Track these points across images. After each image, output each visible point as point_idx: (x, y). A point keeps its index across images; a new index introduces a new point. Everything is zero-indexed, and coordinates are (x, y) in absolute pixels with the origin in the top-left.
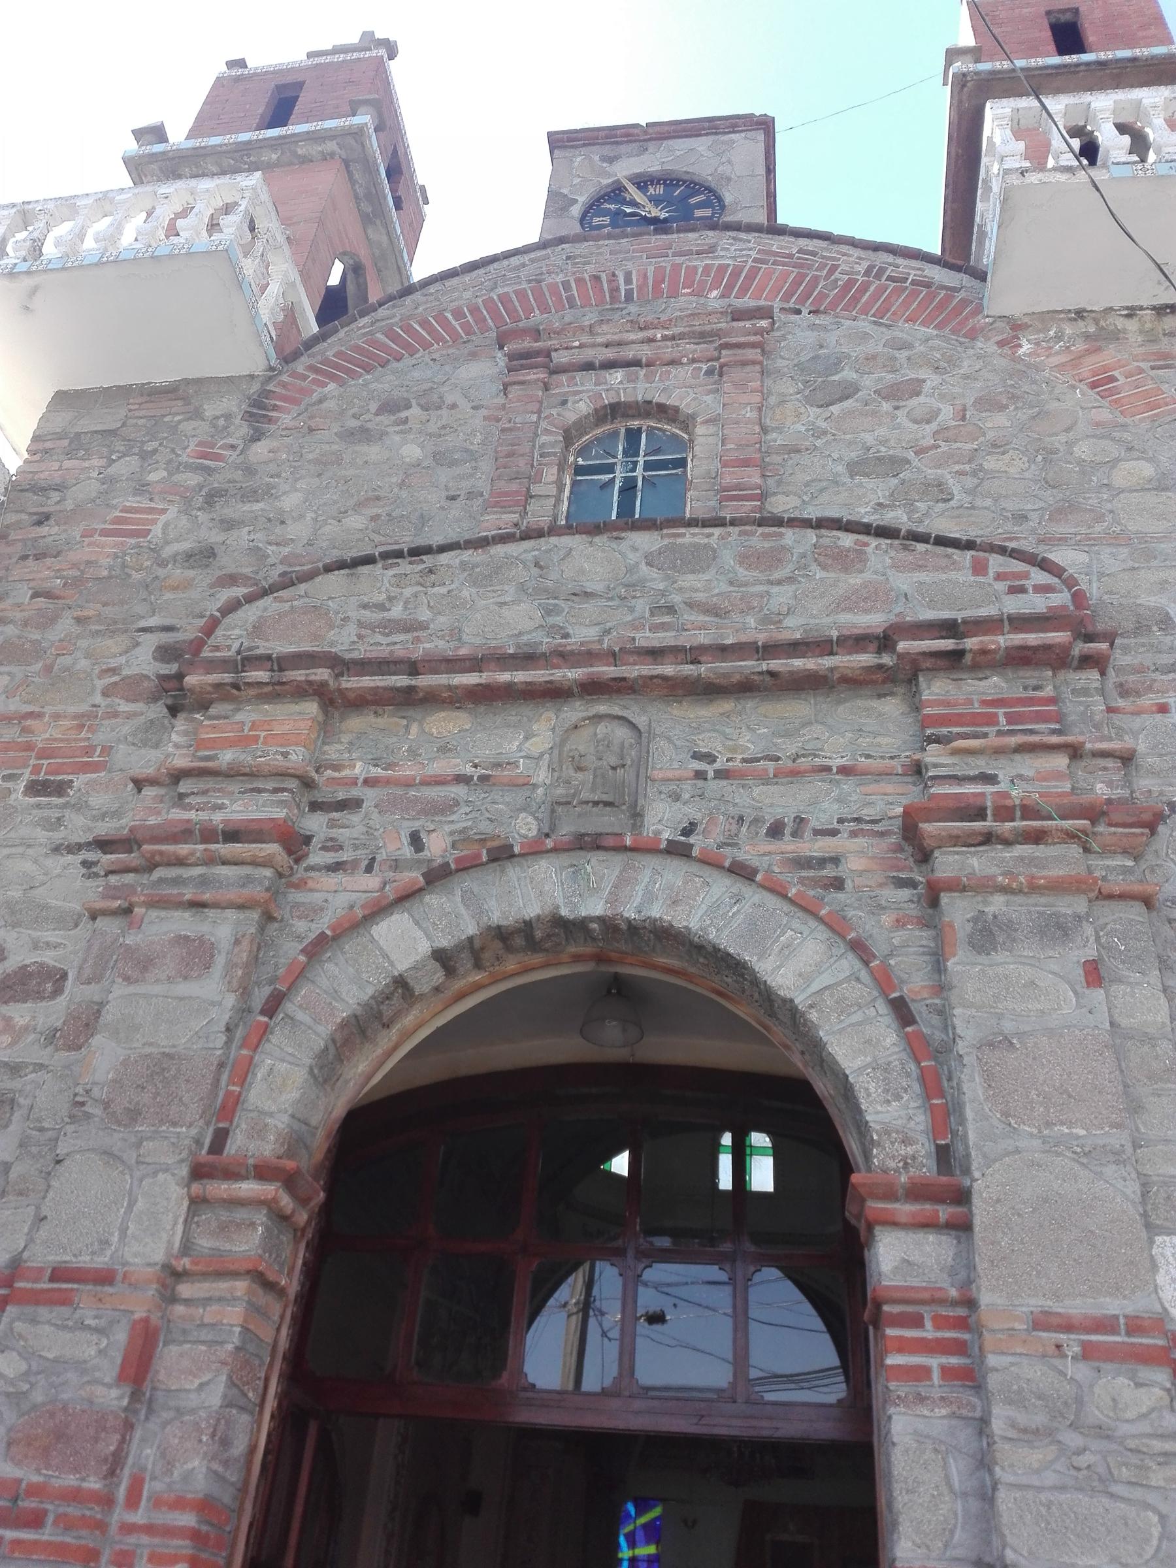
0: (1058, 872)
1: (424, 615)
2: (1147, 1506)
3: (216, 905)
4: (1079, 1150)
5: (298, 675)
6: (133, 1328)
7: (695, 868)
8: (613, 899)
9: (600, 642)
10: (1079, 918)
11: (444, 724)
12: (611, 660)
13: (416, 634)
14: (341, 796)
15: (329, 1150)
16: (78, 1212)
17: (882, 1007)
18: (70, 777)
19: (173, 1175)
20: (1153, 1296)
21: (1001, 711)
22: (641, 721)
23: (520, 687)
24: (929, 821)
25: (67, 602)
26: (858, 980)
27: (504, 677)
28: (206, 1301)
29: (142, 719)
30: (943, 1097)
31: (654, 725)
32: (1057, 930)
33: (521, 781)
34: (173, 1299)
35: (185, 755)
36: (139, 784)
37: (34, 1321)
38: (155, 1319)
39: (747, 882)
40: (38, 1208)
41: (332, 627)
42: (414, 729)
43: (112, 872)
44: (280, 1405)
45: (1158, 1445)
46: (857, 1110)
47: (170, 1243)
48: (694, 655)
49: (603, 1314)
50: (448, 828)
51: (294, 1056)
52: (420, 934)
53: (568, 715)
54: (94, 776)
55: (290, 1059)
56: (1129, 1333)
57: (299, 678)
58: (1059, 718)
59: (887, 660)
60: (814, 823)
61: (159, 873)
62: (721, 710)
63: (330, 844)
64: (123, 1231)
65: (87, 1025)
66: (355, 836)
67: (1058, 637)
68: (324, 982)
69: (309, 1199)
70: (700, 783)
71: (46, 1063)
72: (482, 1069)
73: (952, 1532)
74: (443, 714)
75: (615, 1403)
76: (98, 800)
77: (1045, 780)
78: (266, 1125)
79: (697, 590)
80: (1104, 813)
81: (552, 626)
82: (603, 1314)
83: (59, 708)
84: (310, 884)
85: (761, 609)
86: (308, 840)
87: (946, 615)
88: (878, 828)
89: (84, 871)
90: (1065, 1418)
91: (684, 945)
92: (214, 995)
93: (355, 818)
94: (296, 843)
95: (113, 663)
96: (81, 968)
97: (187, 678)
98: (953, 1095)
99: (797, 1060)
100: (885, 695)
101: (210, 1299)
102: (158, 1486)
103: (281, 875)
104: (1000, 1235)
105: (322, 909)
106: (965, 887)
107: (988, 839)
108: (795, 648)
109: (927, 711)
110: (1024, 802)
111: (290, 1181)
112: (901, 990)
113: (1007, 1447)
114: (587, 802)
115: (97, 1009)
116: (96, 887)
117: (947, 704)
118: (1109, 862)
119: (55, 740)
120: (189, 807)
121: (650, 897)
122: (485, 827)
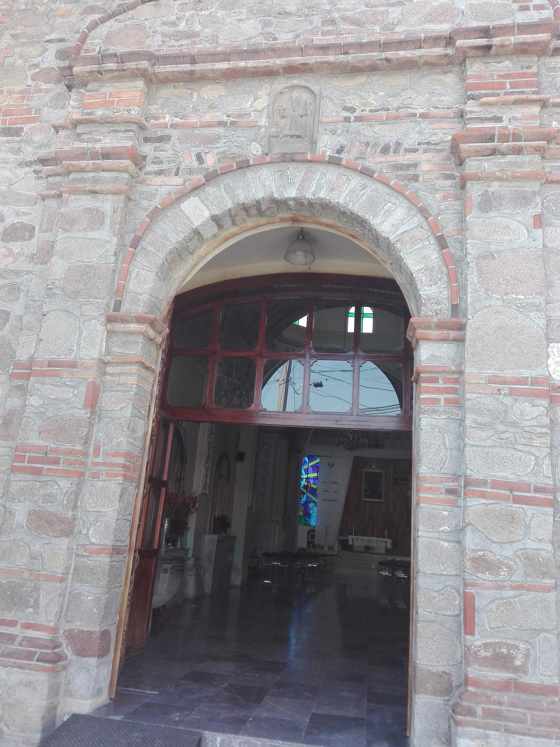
0: (527, 169)
1: (198, 28)
2: (530, 453)
3: (102, 193)
4: (519, 305)
5: (132, 65)
6: (88, 386)
7: (342, 171)
8: (301, 188)
9: (294, 42)
10: (534, 193)
11: (211, 92)
12: (300, 52)
13: (193, 40)
14: (159, 134)
15: (169, 311)
16: (57, 337)
17: (432, 240)
18: (22, 126)
19: (98, 320)
20: (546, 369)
21: (508, 81)
22: (316, 89)
23: (251, 70)
24: (465, 143)
25: (6, 25)
26: (422, 227)
27: (242, 64)
28: (120, 374)
29: (54, 93)
30: (458, 282)
31: (323, 91)
32: (523, 200)
33: (253, 125)
34: (105, 374)
35: (78, 113)
36: (57, 129)
37: (43, 383)
38: (98, 382)
39: (370, 178)
40: (38, 335)
41: (148, 37)
42: (195, 96)
43: (50, 176)
44: (156, 417)
45: (538, 430)
46: (416, 290)
47: (100, 350)
48: (345, 49)
49: (294, 384)
50: (215, 151)
51: (148, 267)
52: (204, 207)
53: (277, 86)
54: (33, 125)
55: (147, 269)
56: (532, 385)
57: (132, 67)
58: (538, 85)
59: (450, 51)
60: (405, 146)
61: (72, 176)
62: (359, 82)
63: (156, 160)
64: (79, 345)
65: (48, 252)
66: (169, 156)
67: (543, 36)
68: (159, 232)
69: (162, 332)
70: (347, 124)
71: (32, 270)
72: (238, 276)
73: (444, 463)
74: (210, 87)
75: (301, 416)
76: (37, 138)
77: (527, 120)
78: (139, 299)
79: (348, 10)
80: (555, 138)
81: (268, 33)
82: (294, 384)
83: (11, 88)
84: (148, 181)
85: (383, 22)
86: (144, 158)
87: (484, 24)
88: (438, 147)
89: (35, 175)
90: (498, 419)
91: (336, 212)
92: (106, 237)
93: (168, 146)
94: (138, 160)
95: (35, 61)
96: (41, 225)
97: (74, 68)
98: (462, 281)
99: (388, 267)
100: (447, 73)
101: (121, 373)
102: (107, 448)
103: (133, 177)
104: (477, 343)
105: (155, 195)
106: (479, 178)
107: (494, 152)
108: (401, 44)
109: (469, 81)
110: (515, 132)
111: (152, 323)
112: (442, 231)
113: (472, 430)
114: (287, 136)
115: (52, 244)
116: (42, 184)
117: (480, 77)
118: (554, 164)
119: (12, 105)
120: (83, 141)
121: (319, 187)
122: (234, 150)
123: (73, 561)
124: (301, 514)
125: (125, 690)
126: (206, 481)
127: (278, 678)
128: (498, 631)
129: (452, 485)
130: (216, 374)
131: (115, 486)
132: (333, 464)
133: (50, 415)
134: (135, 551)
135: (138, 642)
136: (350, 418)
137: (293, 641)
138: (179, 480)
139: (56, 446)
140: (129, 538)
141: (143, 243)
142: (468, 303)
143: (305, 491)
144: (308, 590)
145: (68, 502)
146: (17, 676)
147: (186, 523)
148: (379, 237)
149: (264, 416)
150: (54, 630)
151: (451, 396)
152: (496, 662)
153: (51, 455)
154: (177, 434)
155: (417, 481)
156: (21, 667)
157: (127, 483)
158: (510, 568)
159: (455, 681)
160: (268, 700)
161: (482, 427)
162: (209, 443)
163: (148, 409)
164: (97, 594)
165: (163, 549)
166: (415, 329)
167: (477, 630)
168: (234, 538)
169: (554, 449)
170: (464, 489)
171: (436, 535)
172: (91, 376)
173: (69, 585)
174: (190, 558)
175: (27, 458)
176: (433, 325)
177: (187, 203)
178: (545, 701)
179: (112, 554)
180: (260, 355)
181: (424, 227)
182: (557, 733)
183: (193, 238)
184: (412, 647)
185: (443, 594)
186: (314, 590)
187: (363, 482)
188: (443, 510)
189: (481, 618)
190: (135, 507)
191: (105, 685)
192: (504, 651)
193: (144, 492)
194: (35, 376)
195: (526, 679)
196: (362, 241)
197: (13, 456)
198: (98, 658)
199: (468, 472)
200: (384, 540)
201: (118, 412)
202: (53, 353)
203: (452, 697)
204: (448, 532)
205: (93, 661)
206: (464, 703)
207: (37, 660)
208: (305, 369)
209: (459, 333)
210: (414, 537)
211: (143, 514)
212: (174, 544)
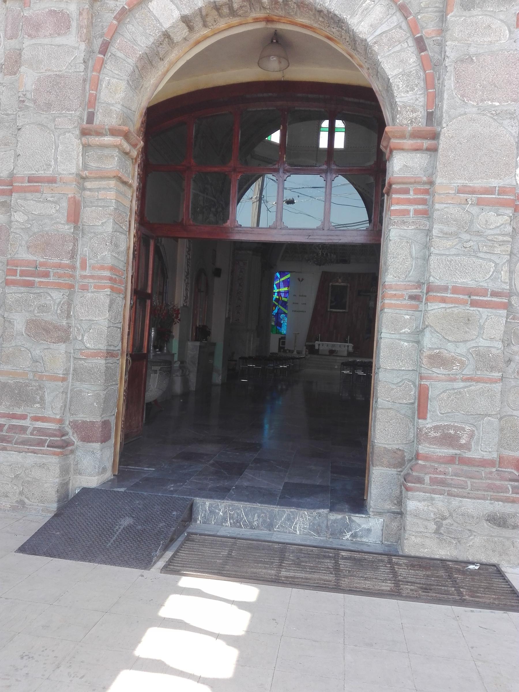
15: (142, 123)
17: (411, 42)
19: (73, 134)
20: (514, 178)
26: (400, 27)
28: (99, 189)
30: (434, 88)
34: (84, 189)
37: (25, 199)
38: (78, 197)
44: (137, 232)
45: (501, 238)
47: (77, 164)
49: (267, 202)
51: (119, 75)
52: (173, 7)
55: (117, 77)
56: (499, 195)
64: (56, 160)
65: (16, 61)
68: (128, 35)
72: (210, 85)
73: (409, 272)
75: (275, 231)
78: (111, 110)
82: (267, 202)
90: (464, 228)
91: (312, 11)
98: (439, 87)
99: (364, 72)
101: (100, 188)
102: (92, 262)
111: (126, 136)
115: (19, 52)
123: (72, 364)
124: (273, 324)
125: (126, 468)
126: (187, 294)
127: (256, 456)
128: (448, 416)
129: (415, 292)
130: (191, 190)
131: (103, 296)
132: (303, 279)
133: (36, 230)
134: (127, 355)
135: (135, 430)
136: (321, 232)
137: (267, 426)
138: (161, 294)
139: (44, 260)
140: (121, 343)
141: (112, 48)
142: (444, 110)
143: (277, 304)
144: (280, 387)
145: (62, 312)
146: (30, 459)
147: (170, 332)
148: (356, 39)
149: (239, 232)
150: (61, 421)
151: (420, 207)
152: (444, 441)
153: (41, 269)
154: (157, 251)
155: (383, 289)
156: (34, 452)
157: (114, 294)
158: (462, 363)
159: (407, 457)
160: (248, 473)
161: (448, 236)
162: (188, 259)
163: (128, 223)
164: (96, 391)
165: (152, 354)
166: (390, 139)
167: (428, 415)
168: (214, 344)
169: (513, 256)
170: (426, 294)
171: (398, 336)
172: (71, 191)
173: (70, 385)
174: (176, 362)
175: (18, 275)
176: (408, 135)
177: (155, 3)
178: (483, 472)
179: (107, 357)
180: (235, 170)
181: (403, 28)
182: (491, 496)
183: (163, 41)
184: (371, 429)
185: (400, 386)
186: (284, 387)
187: (330, 294)
188: (405, 315)
189: (433, 406)
190: (124, 316)
191: (109, 465)
192: (452, 432)
193: (131, 303)
194: (17, 192)
195: (468, 455)
196: (338, 43)
197: (5, 270)
198: (101, 443)
199: (432, 279)
200: (347, 344)
201: (100, 228)
202: (32, 169)
203: (404, 469)
204: (409, 333)
205: (97, 446)
206: (414, 474)
207: (48, 446)
208: (278, 187)
209: (433, 142)
210: (377, 338)
211: (132, 323)
212: (161, 349)
